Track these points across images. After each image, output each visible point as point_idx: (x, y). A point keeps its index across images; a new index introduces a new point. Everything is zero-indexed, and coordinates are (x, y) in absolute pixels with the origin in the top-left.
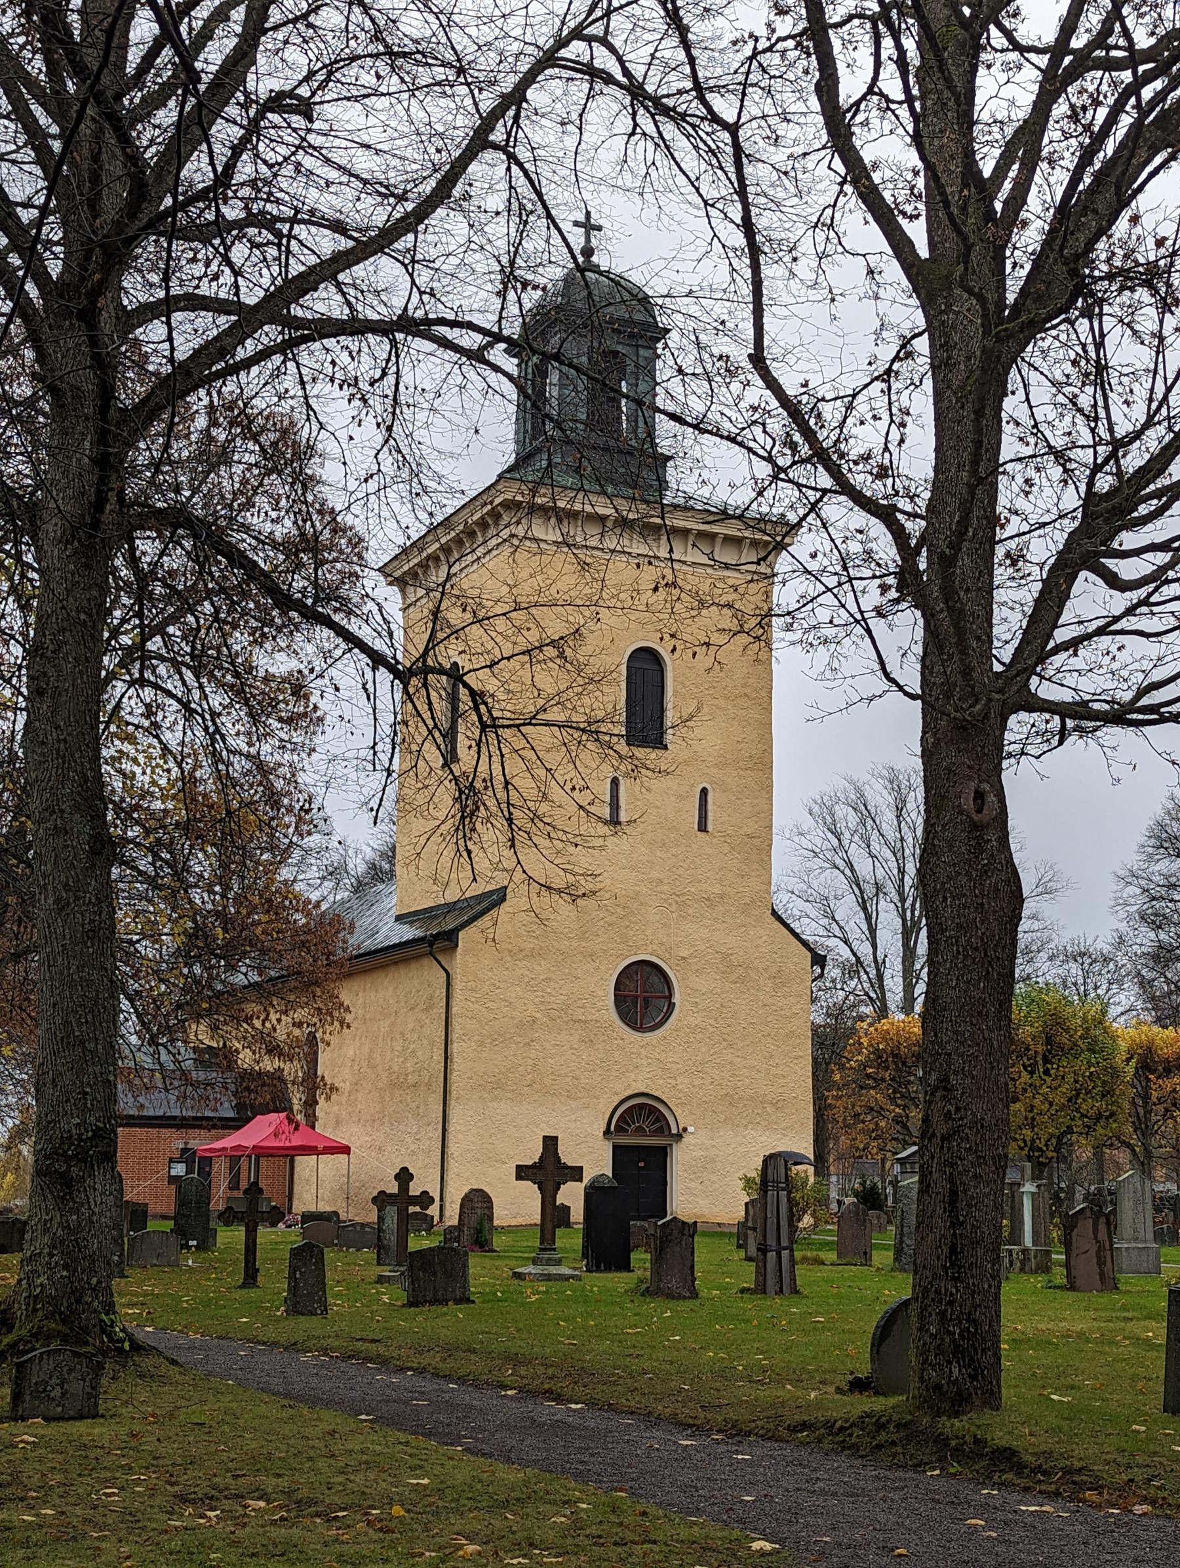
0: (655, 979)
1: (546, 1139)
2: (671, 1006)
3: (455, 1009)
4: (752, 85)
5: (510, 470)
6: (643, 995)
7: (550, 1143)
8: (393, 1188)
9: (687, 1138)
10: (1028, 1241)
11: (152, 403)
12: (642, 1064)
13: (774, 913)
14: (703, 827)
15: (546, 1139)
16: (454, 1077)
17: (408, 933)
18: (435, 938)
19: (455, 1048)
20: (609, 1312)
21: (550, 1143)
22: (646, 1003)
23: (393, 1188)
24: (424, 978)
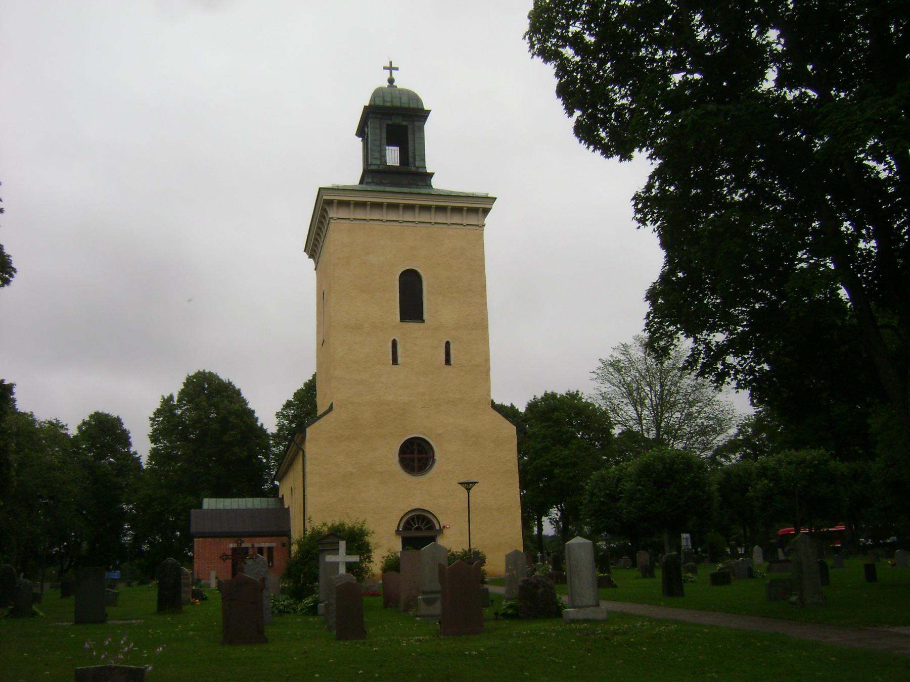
6: (416, 456)
14: (448, 361)
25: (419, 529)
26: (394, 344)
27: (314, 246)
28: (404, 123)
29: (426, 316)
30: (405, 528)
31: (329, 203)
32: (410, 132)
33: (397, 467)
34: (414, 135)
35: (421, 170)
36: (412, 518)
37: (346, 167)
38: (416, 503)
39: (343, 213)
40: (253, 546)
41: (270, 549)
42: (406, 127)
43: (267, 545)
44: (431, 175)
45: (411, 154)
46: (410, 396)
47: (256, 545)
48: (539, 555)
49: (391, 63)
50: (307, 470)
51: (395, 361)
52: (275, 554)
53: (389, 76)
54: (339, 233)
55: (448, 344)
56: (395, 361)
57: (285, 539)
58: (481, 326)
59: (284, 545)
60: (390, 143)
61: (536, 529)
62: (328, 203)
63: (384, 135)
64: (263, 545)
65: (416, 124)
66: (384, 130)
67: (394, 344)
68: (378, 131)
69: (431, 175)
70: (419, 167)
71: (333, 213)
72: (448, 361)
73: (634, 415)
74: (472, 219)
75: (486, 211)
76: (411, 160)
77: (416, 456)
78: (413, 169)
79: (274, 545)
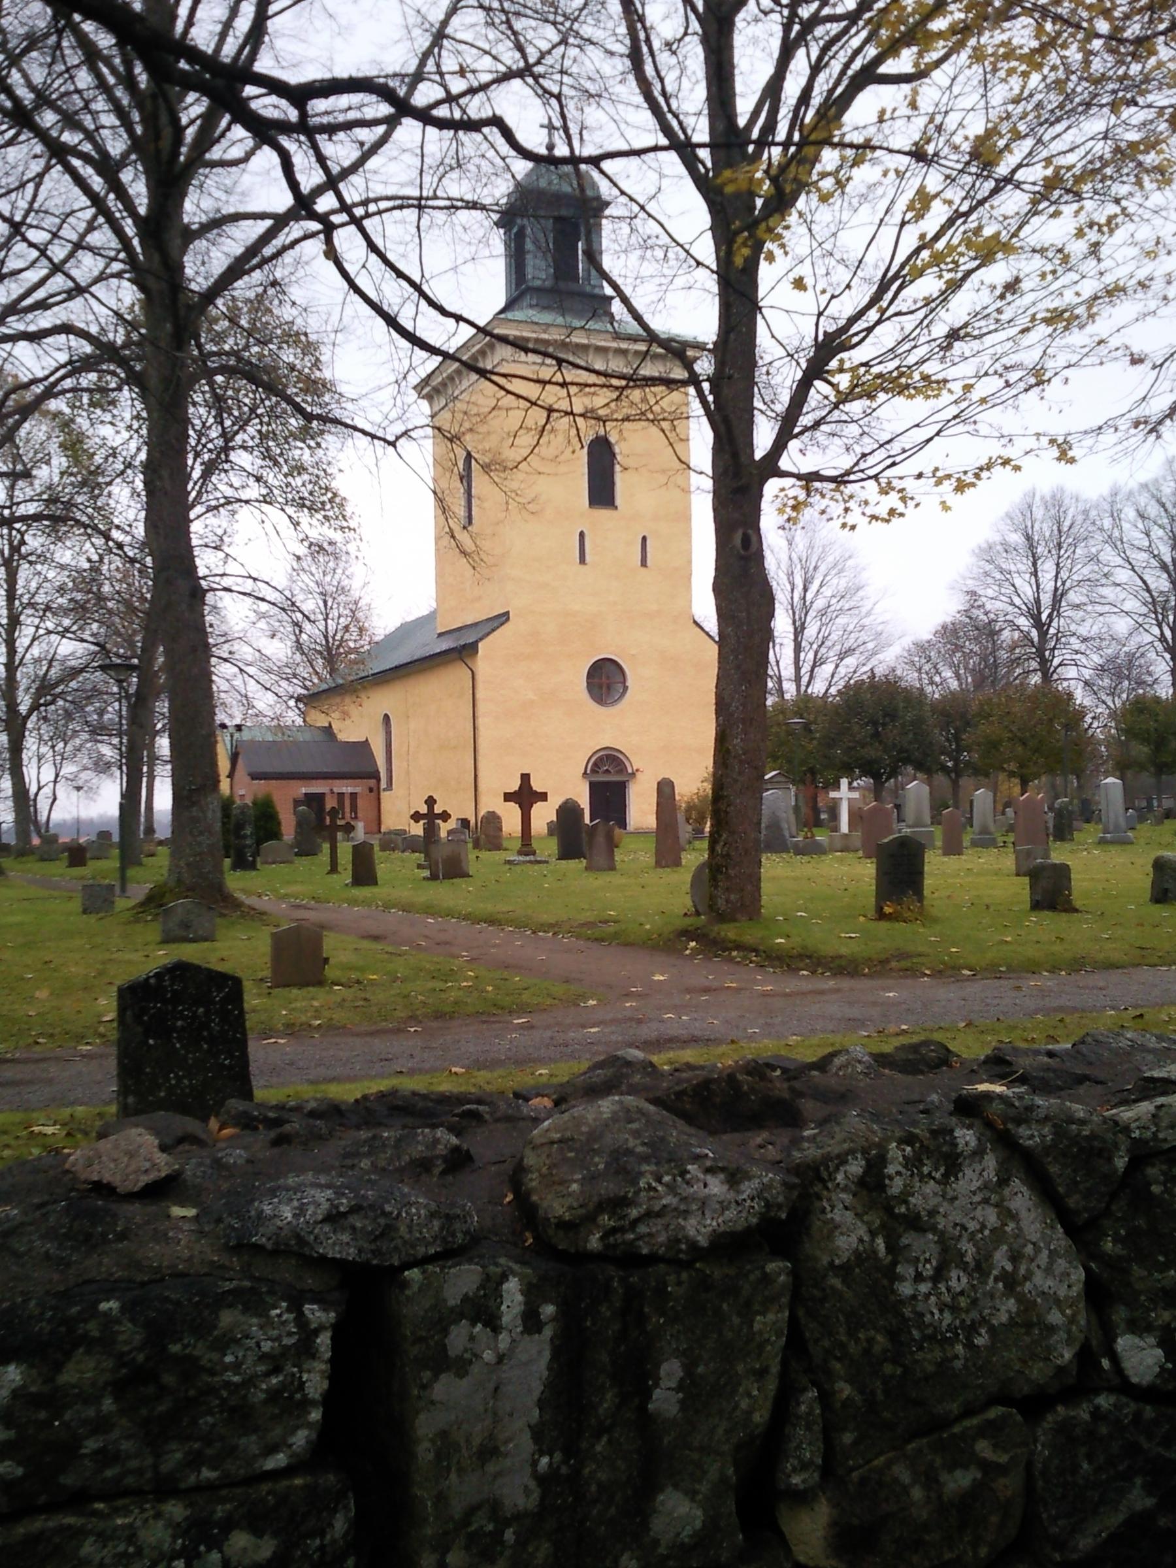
0: (613, 667)
1: (522, 775)
2: (626, 688)
3: (478, 696)
4: (90, 249)
5: (502, 311)
6: (605, 680)
7: (525, 778)
8: (424, 809)
9: (638, 775)
10: (844, 827)
11: (816, 100)
12: (610, 728)
13: (695, 622)
14: (644, 563)
15: (522, 775)
16: (480, 741)
17: (444, 645)
18: (460, 650)
19: (480, 721)
20: (576, 888)
21: (525, 778)
22: (609, 687)
23: (424, 809)
24: (456, 675)
26: (582, 535)
29: (619, 501)
30: (593, 771)
33: (585, 695)
36: (601, 758)
38: (607, 740)
40: (332, 792)
41: (354, 796)
43: (350, 790)
47: (336, 790)
48: (91, 1445)
51: (582, 560)
53: (547, 140)
55: (644, 539)
56: (582, 560)
57: (372, 782)
59: (371, 790)
61: (1105, 1363)
64: (344, 790)
67: (582, 535)
70: (594, 287)
72: (644, 563)
77: (605, 680)
78: (588, 289)
79: (358, 790)
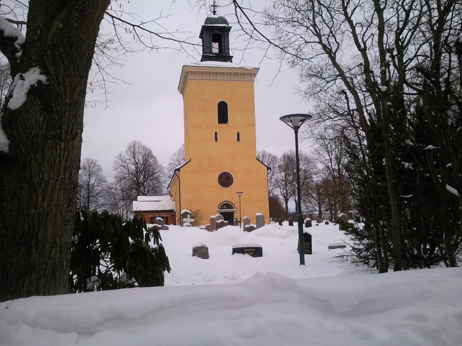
6: (226, 180)
25: (361, 74)
26: (216, 134)
27: (182, 89)
28: (220, 33)
31: (188, 72)
32: (223, 37)
34: (224, 38)
35: (228, 55)
37: (194, 55)
39: (193, 77)
41: (167, 218)
42: (221, 35)
43: (166, 216)
44: (232, 57)
45: (223, 47)
46: (223, 154)
49: (214, 2)
50: (181, 185)
51: (216, 139)
52: (169, 219)
54: (191, 84)
56: (216, 139)
57: (173, 213)
58: (253, 125)
59: (172, 215)
60: (215, 42)
62: (187, 74)
63: (211, 39)
65: (226, 33)
66: (211, 37)
67: (216, 134)
68: (208, 37)
69: (232, 57)
70: (226, 54)
71: (190, 77)
73: (328, 158)
74: (249, 78)
75: (255, 75)
76: (223, 50)
77: (226, 180)
79: (168, 216)
